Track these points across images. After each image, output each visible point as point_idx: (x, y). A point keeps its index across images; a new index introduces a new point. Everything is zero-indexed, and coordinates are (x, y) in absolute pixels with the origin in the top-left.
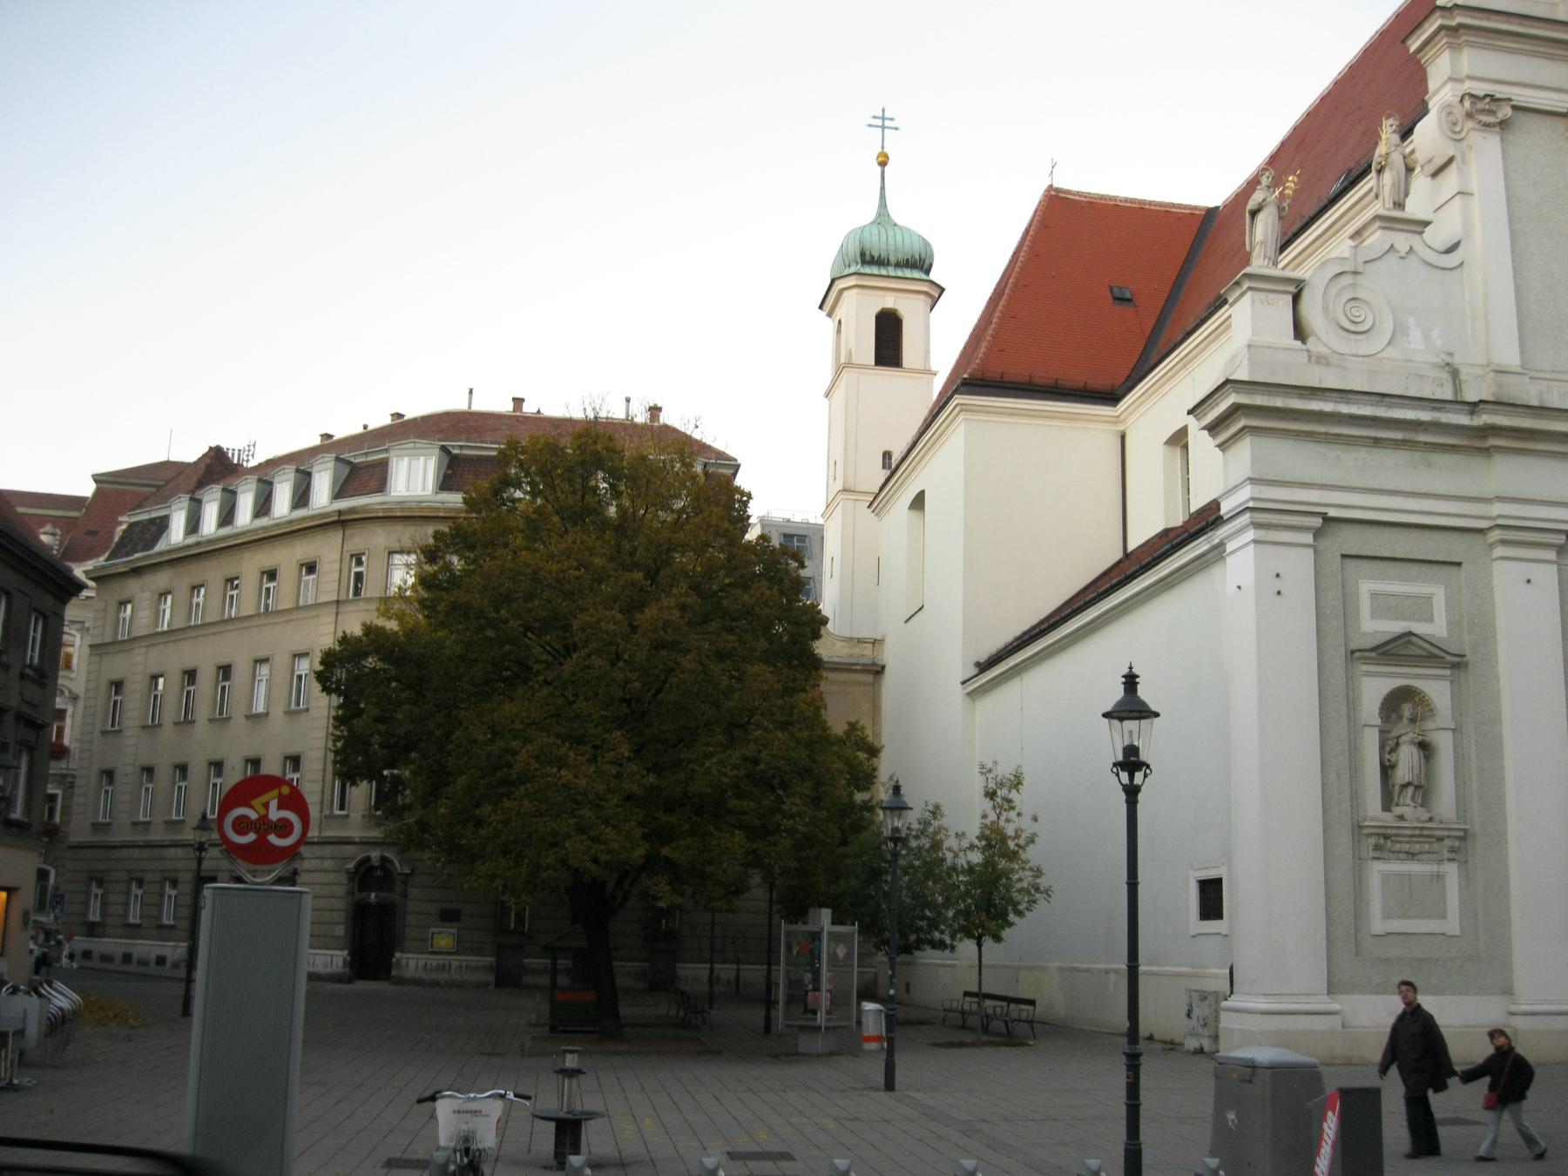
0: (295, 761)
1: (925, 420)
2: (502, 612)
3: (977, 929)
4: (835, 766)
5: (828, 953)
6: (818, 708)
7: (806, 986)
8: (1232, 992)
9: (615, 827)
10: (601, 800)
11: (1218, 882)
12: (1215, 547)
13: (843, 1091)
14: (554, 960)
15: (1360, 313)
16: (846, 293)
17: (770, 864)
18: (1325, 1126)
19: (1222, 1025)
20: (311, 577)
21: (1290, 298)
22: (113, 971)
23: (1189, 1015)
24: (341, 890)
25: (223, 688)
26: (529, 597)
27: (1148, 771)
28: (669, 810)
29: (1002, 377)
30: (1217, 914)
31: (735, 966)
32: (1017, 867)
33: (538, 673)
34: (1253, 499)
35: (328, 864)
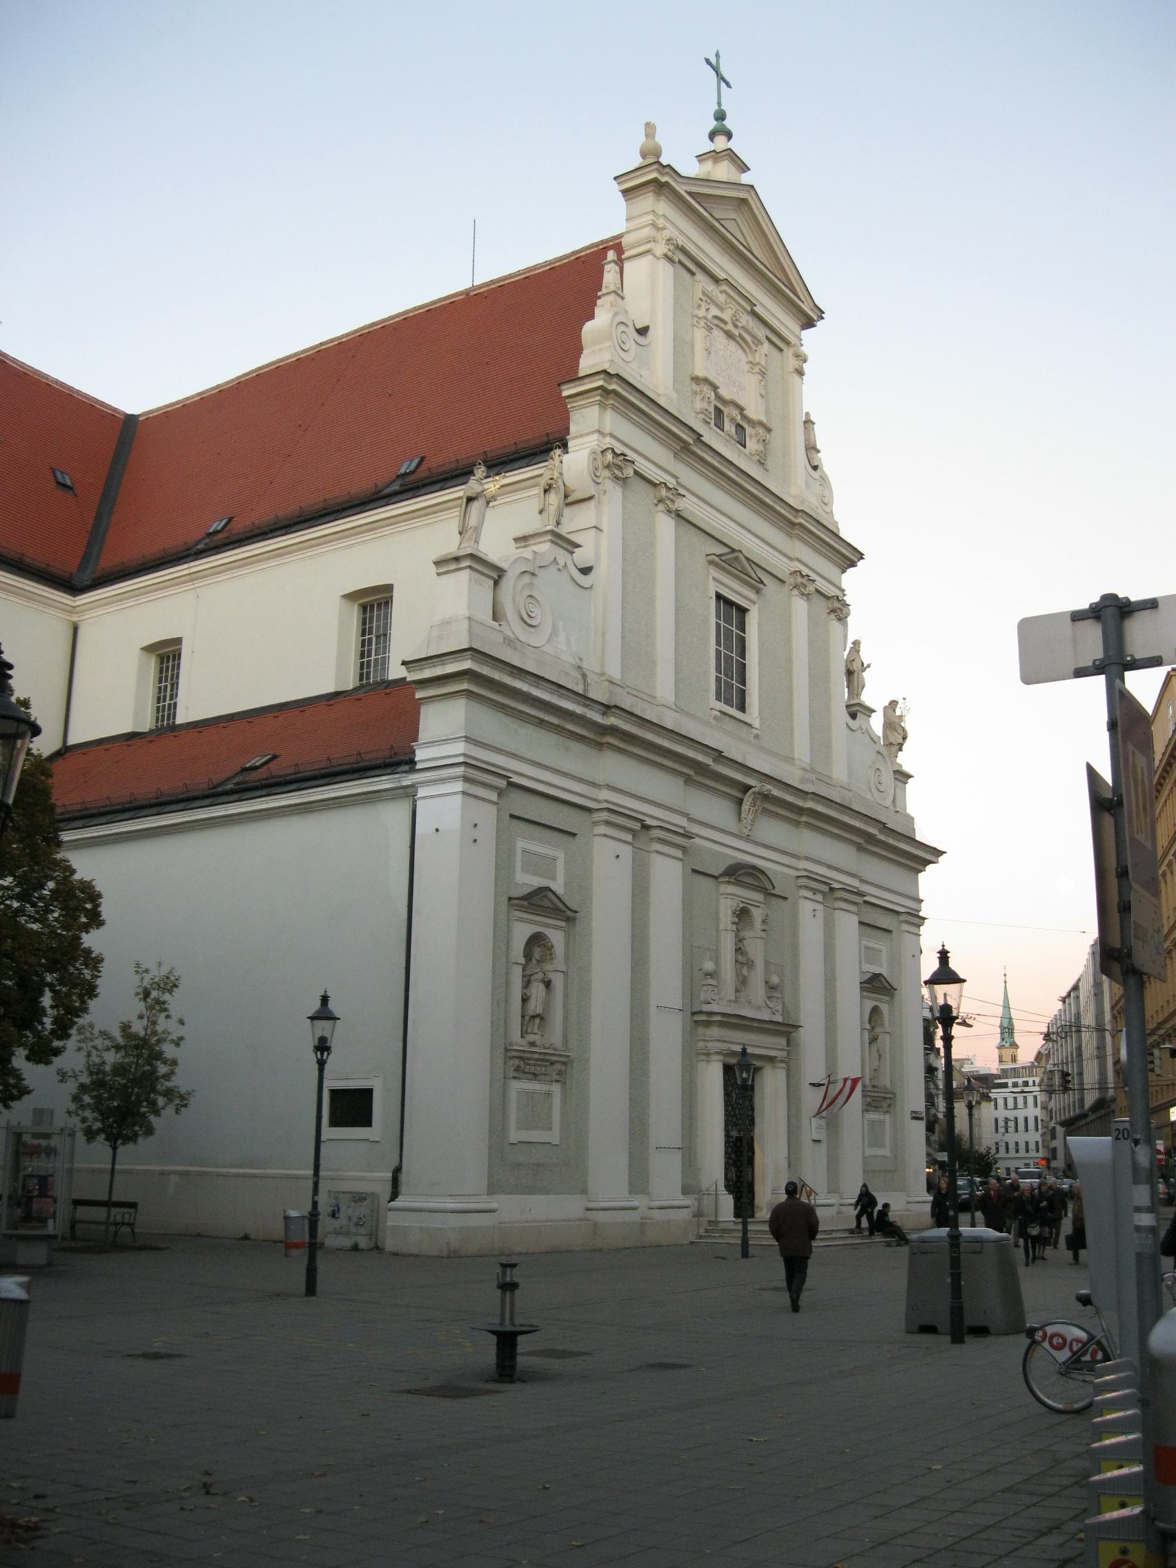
15: (536, 612)
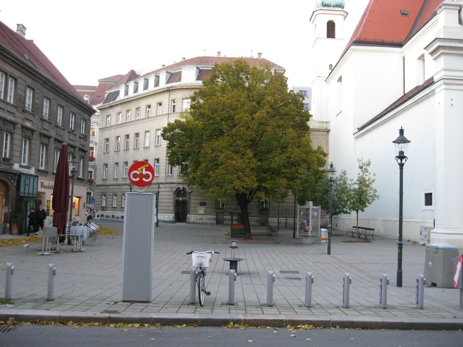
0: (158, 160)
1: (342, 54)
2: (214, 115)
3: (356, 208)
4: (314, 159)
5: (312, 215)
6: (308, 142)
7: (305, 224)
8: (434, 227)
9: (249, 178)
10: (244, 170)
11: (431, 194)
12: (432, 91)
13: (315, 254)
14: (232, 216)
16: (317, 16)
17: (294, 188)
18: (457, 266)
19: (431, 237)
20: (160, 107)
21: (457, 11)
22: (109, 220)
23: (421, 234)
24: (172, 197)
25: (137, 139)
26: (222, 110)
27: (407, 159)
28: (265, 173)
29: (366, 40)
30: (431, 204)
31: (285, 219)
32: (369, 189)
33: (225, 133)
34: (444, 76)
35: (168, 189)
